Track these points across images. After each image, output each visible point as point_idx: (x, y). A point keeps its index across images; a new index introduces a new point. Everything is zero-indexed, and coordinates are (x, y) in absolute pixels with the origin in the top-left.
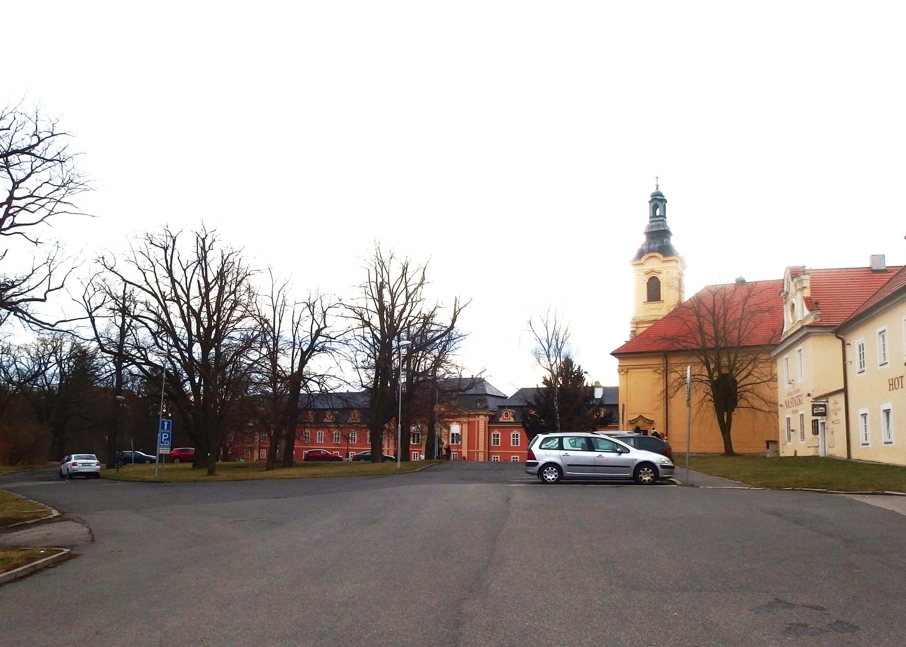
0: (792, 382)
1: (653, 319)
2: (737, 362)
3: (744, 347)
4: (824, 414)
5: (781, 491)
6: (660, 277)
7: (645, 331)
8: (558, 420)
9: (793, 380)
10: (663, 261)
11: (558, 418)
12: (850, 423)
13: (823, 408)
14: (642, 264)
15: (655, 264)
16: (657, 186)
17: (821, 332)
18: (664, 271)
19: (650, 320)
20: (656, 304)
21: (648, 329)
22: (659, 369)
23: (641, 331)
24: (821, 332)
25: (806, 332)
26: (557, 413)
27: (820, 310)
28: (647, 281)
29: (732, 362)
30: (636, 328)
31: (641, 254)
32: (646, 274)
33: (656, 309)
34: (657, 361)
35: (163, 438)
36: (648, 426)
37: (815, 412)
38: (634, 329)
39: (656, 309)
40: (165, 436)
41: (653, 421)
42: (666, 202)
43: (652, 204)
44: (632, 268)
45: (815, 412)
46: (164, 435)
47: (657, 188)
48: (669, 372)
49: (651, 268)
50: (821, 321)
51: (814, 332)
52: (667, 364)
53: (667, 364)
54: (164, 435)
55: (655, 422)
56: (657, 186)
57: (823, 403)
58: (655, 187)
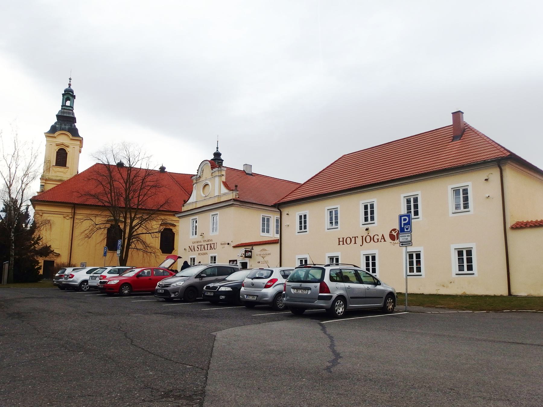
0: (202, 234)
1: (58, 179)
2: (135, 218)
3: (141, 209)
4: (250, 257)
5: (502, 313)
6: (67, 150)
7: (54, 188)
8: (13, 249)
9: (203, 234)
10: (72, 139)
11: (13, 247)
12: (509, 264)
13: (250, 253)
14: (55, 137)
15: (64, 139)
16: (70, 85)
17: (239, 205)
18: (71, 146)
19: (57, 179)
20: (63, 169)
21: (56, 186)
22: (68, 216)
23: (49, 187)
24: (239, 205)
25: (232, 203)
26: (13, 243)
27: (238, 190)
28: (57, 151)
29: (132, 218)
30: (45, 183)
31: (53, 129)
32: (57, 145)
33: (62, 172)
34: (69, 210)
35: (403, 222)
36: (55, 258)
37: (246, 255)
38: (43, 184)
39: (62, 172)
40: (405, 220)
41: (59, 254)
42: (75, 98)
43: (65, 97)
44: (44, 139)
45: (246, 255)
46: (404, 219)
47: (69, 87)
48: (75, 219)
49: (62, 142)
50: (239, 198)
51: (236, 204)
52: (74, 213)
53: (74, 213)
54: (404, 219)
55: (61, 254)
56: (70, 85)
57: (250, 250)
58: (68, 86)
